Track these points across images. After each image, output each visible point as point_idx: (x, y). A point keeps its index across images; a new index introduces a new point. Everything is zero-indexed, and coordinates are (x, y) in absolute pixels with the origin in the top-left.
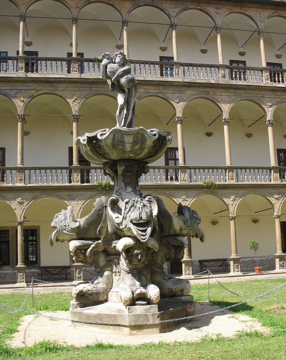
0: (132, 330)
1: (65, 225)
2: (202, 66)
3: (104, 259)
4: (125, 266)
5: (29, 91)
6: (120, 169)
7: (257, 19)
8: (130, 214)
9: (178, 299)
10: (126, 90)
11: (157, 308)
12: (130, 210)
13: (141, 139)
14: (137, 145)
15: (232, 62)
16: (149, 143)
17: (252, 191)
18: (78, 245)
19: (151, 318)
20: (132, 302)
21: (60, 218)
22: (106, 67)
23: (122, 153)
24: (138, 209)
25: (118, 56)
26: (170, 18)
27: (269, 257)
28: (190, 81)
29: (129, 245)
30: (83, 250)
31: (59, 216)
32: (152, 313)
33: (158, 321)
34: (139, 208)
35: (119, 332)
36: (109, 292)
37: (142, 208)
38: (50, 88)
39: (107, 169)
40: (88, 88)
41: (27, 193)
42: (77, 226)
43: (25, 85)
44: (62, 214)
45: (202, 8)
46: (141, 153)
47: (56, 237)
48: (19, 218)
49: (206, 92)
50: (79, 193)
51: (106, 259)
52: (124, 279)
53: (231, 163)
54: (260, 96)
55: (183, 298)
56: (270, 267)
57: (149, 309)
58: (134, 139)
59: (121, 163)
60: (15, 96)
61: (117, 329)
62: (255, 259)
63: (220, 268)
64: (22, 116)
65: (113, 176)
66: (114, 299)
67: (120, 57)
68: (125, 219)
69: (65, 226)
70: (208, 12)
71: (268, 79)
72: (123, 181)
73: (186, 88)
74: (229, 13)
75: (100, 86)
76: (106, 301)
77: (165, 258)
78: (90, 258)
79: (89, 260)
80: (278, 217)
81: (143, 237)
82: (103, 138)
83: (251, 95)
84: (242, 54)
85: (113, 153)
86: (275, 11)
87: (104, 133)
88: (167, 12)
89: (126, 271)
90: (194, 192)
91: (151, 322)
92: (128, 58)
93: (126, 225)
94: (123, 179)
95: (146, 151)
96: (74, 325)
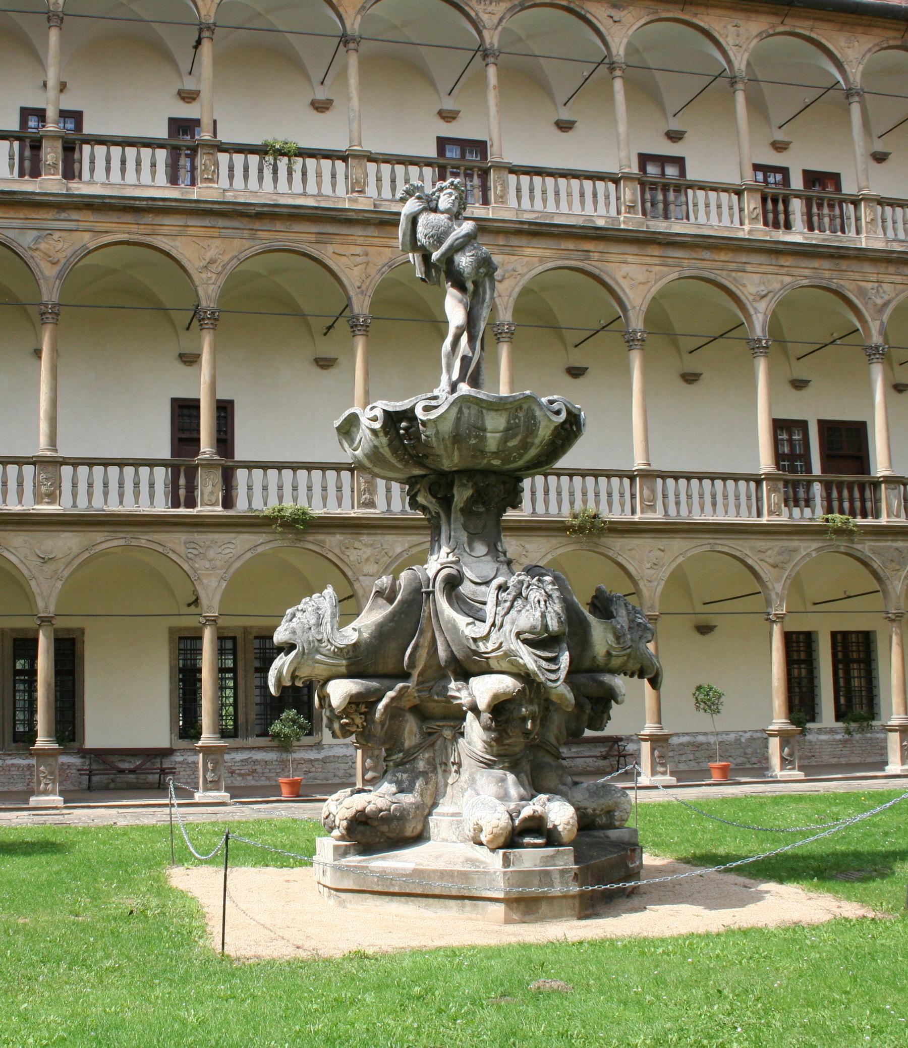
0: (511, 909)
1: (319, 637)
2: (569, 175)
3: (415, 729)
4: (479, 747)
5: (75, 233)
6: (461, 495)
7: (728, 42)
8: (500, 617)
9: (600, 837)
10: (470, 286)
11: (572, 854)
12: (512, 607)
13: (525, 422)
14: (514, 436)
15: (644, 159)
16: (544, 432)
17: (706, 542)
18: (354, 692)
19: (557, 879)
20: (512, 839)
21: (305, 621)
22: (414, 220)
23: (473, 456)
24: (537, 605)
25: (445, 192)
26: (479, 32)
27: (741, 734)
28: (537, 218)
29: (505, 694)
30: (363, 706)
31: (299, 615)
32: (561, 868)
33: (575, 889)
34: (539, 602)
35: (474, 916)
36: (430, 814)
37: (545, 602)
38: (136, 226)
39: (422, 493)
40: (245, 232)
41: (67, 534)
42: (353, 642)
43: (63, 215)
44: (310, 609)
45: (572, 6)
46: (521, 456)
47: (292, 669)
48: (40, 604)
49: (579, 253)
50: (216, 536)
51: (421, 728)
52: (473, 781)
53: (648, 459)
54: (732, 266)
55: (613, 834)
56: (743, 764)
57: (552, 857)
58: (508, 422)
59: (465, 482)
60: (34, 247)
61: (468, 908)
62: (701, 739)
63: (601, 763)
64: (54, 306)
65: (438, 514)
66: (443, 834)
67: (451, 194)
68: (499, 630)
69: (320, 641)
70: (588, 16)
71: (756, 218)
72: (465, 527)
73: (523, 241)
74: (648, 20)
75: (279, 226)
76: (420, 838)
77: (567, 729)
78: (383, 725)
79: (378, 731)
80: (778, 618)
81: (553, 677)
82: (432, 418)
83: (707, 264)
84: (674, 136)
85: (451, 456)
86: (781, 19)
87: (433, 403)
88: (473, 14)
89: (482, 762)
90: (543, 540)
91: (557, 890)
92: (360, 145)
93: (501, 643)
94: (465, 522)
95: (533, 452)
96: (340, 902)
